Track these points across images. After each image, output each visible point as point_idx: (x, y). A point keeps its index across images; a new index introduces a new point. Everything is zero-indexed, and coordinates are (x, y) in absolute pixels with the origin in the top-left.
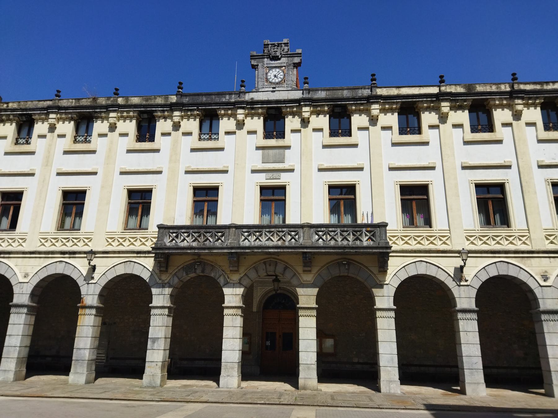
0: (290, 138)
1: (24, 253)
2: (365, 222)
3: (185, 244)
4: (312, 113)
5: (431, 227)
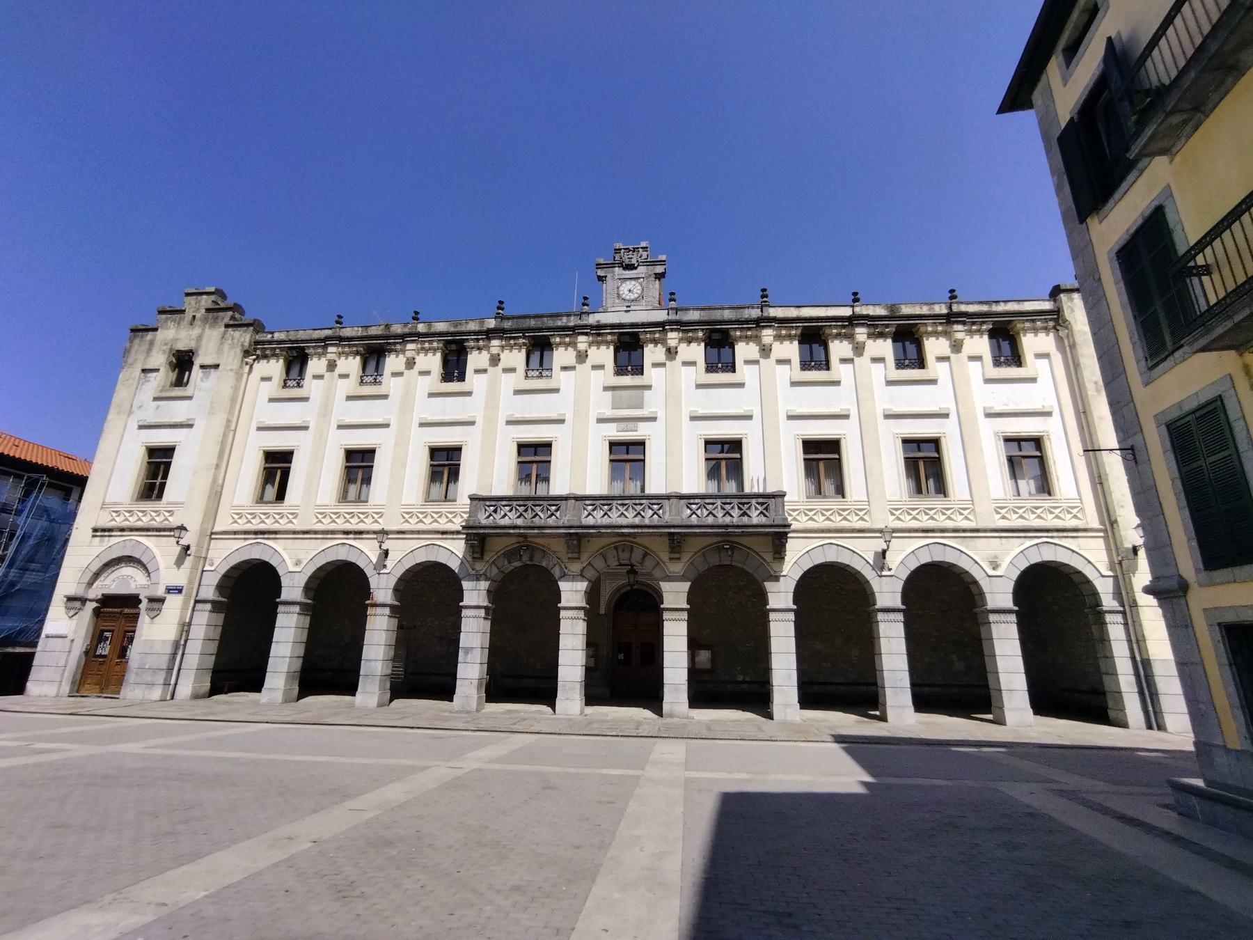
0: (652, 375)
1: (295, 532)
2: (755, 490)
3: (506, 522)
4: (681, 340)
5: (843, 497)
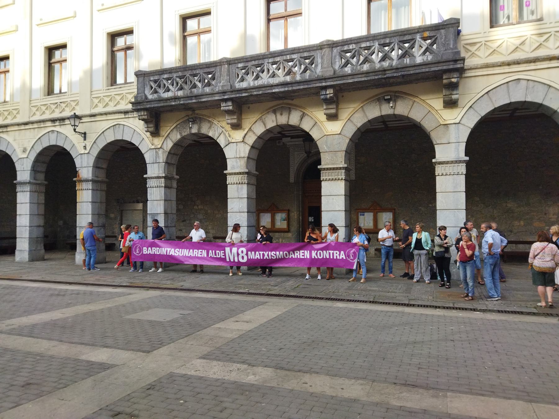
1: (18, 125)
